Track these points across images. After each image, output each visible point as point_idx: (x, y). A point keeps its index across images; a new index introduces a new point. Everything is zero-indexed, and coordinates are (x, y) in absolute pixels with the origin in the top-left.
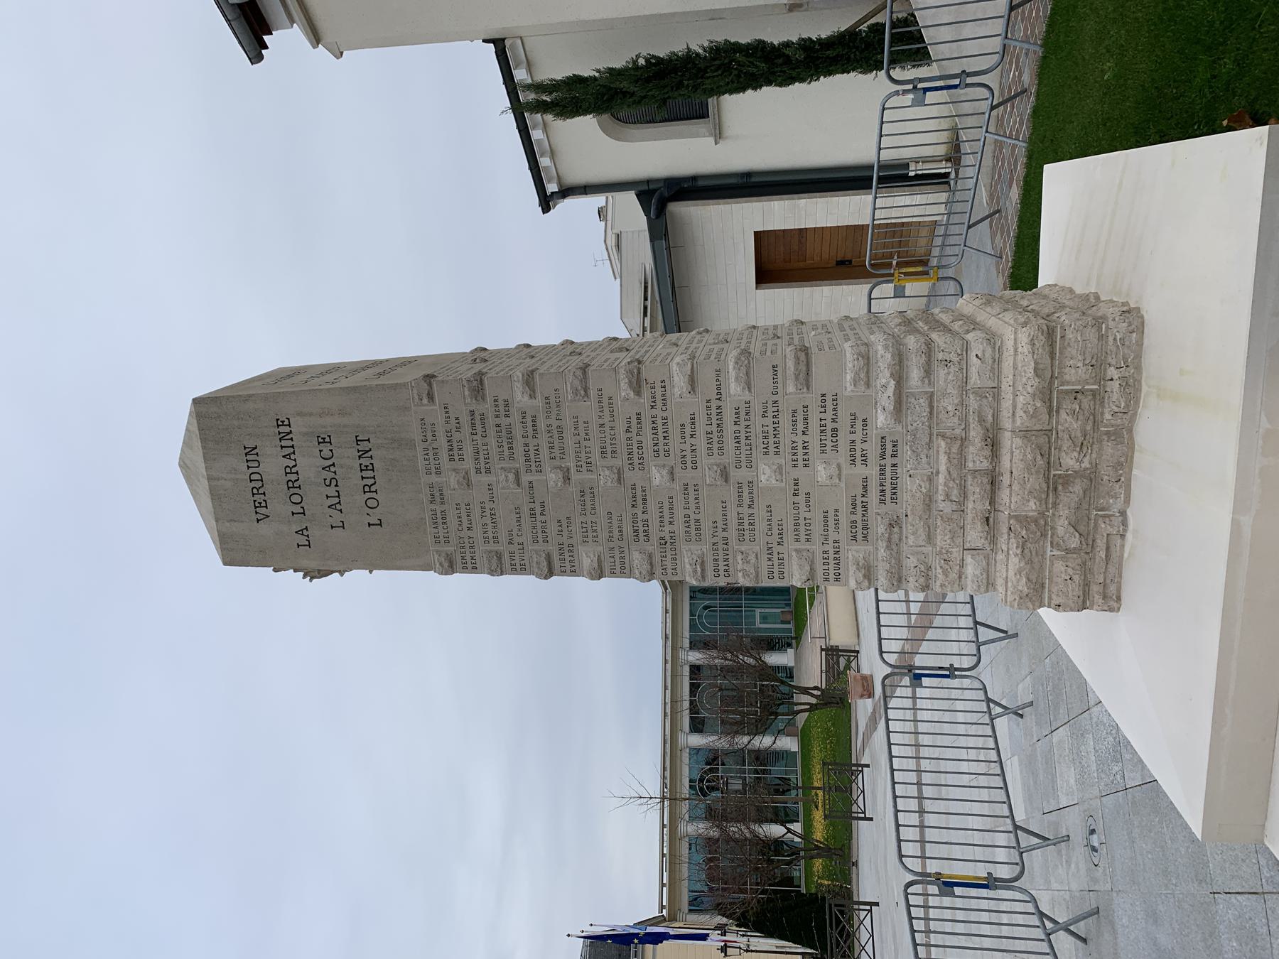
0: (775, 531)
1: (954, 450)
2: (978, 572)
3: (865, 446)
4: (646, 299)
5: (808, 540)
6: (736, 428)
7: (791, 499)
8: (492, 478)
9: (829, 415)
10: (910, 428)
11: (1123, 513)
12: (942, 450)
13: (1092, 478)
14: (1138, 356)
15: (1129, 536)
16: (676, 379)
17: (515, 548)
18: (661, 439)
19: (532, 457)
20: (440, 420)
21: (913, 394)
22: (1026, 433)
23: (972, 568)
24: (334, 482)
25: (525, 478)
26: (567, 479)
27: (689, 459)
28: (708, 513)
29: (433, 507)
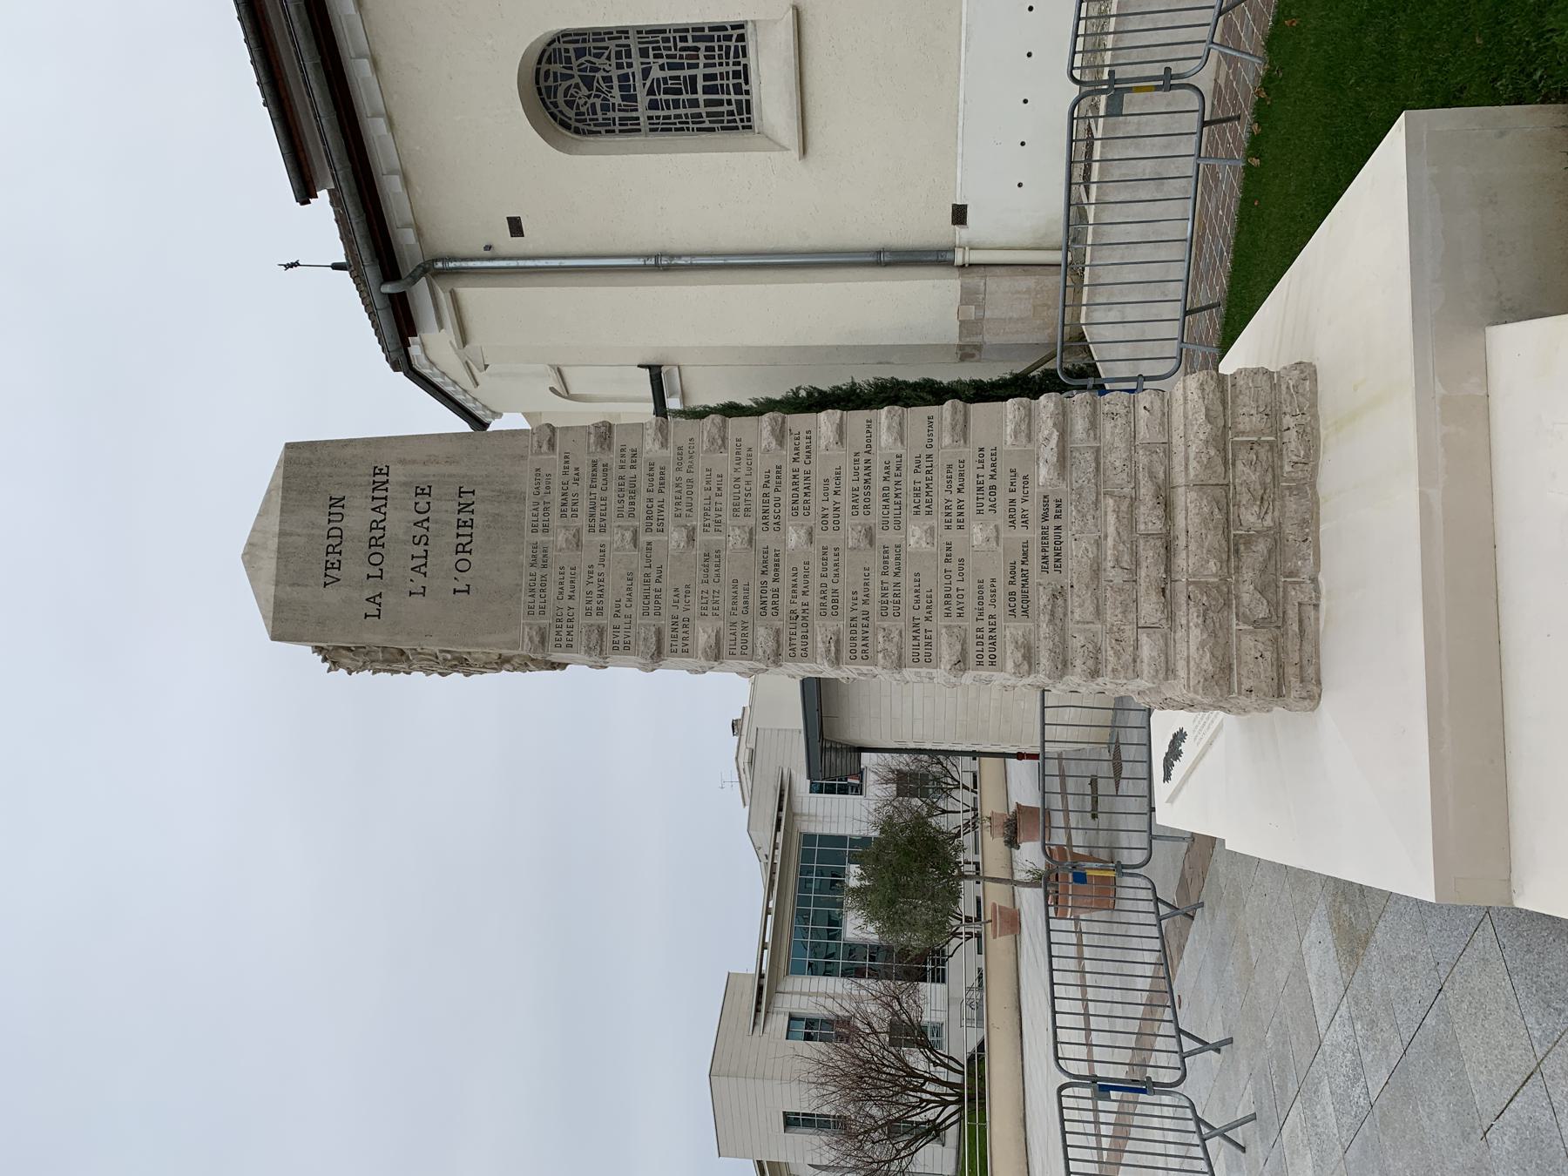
0: (923, 604)
1: (1124, 507)
2: (1155, 654)
3: (1026, 506)
4: (780, 809)
5: (960, 615)
6: (885, 484)
7: (943, 566)
8: (605, 538)
9: (987, 471)
10: (1075, 486)
11: (1314, 580)
12: (1110, 510)
13: (1276, 538)
14: (1314, 405)
15: (1323, 604)
16: (823, 429)
17: (620, 621)
18: (801, 495)
19: (655, 515)
20: (559, 471)
21: (1077, 449)
22: (1201, 486)
23: (1148, 649)
24: (424, 540)
25: (644, 538)
26: (691, 539)
27: (830, 519)
28: (849, 581)
29: (533, 570)
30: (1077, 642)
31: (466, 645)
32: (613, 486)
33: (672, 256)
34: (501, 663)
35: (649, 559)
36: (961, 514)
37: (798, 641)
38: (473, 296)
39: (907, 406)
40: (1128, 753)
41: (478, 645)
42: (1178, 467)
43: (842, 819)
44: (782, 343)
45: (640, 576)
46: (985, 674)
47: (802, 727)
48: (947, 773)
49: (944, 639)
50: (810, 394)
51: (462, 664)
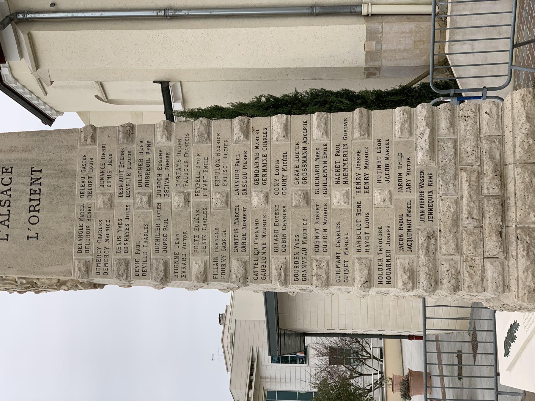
1: (473, 178)
2: (496, 275)
3: (409, 177)
4: (251, 374)
5: (367, 251)
8: (129, 201)
9: (383, 155)
12: (464, 180)
16: (275, 127)
17: (140, 257)
19: (163, 184)
22: (524, 164)
23: (491, 272)
25: (155, 201)
26: (187, 201)
27: (280, 187)
28: (293, 229)
29: (81, 223)
30: (444, 268)
31: (36, 274)
32: (135, 166)
33: (175, 10)
34: (60, 285)
35: (159, 214)
36: (366, 183)
37: (259, 270)
38: (43, 36)
39: (330, 111)
40: (481, 336)
41: (43, 273)
42: (509, 152)
43: (293, 380)
44: (247, 66)
45: (153, 226)
46: (384, 289)
47: (264, 318)
48: (363, 348)
49: (357, 266)
50: (268, 100)
51: (33, 286)
